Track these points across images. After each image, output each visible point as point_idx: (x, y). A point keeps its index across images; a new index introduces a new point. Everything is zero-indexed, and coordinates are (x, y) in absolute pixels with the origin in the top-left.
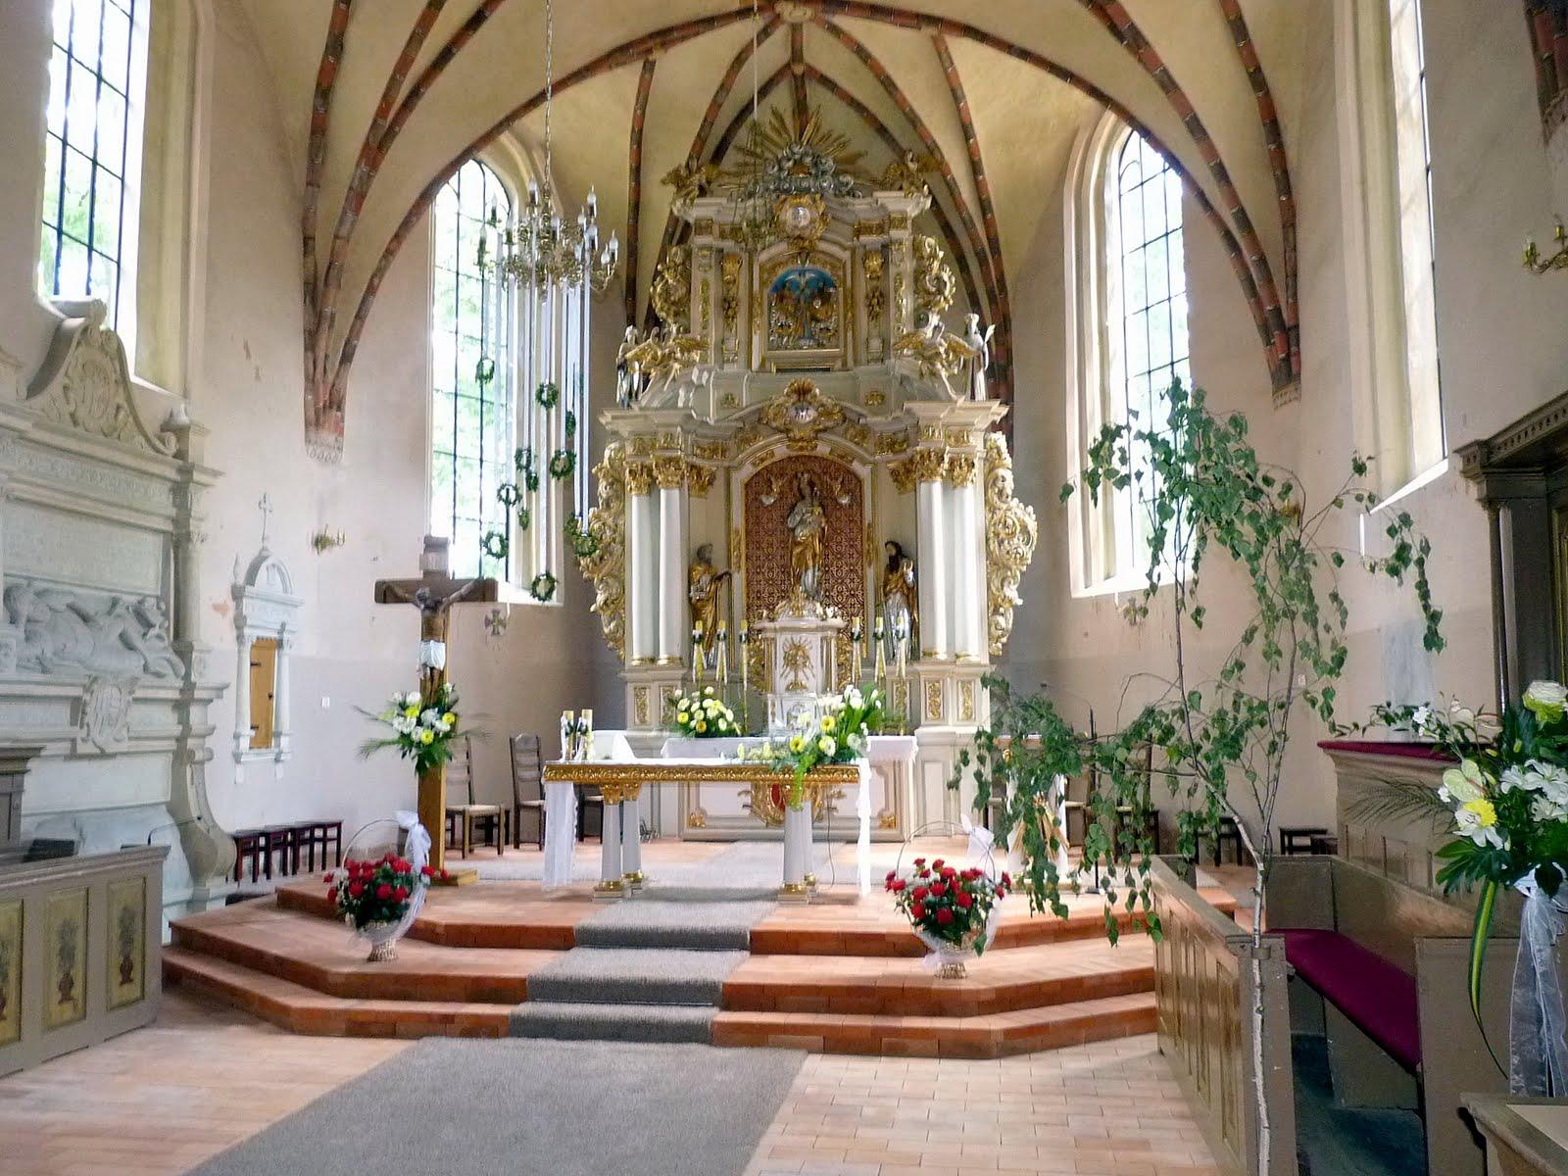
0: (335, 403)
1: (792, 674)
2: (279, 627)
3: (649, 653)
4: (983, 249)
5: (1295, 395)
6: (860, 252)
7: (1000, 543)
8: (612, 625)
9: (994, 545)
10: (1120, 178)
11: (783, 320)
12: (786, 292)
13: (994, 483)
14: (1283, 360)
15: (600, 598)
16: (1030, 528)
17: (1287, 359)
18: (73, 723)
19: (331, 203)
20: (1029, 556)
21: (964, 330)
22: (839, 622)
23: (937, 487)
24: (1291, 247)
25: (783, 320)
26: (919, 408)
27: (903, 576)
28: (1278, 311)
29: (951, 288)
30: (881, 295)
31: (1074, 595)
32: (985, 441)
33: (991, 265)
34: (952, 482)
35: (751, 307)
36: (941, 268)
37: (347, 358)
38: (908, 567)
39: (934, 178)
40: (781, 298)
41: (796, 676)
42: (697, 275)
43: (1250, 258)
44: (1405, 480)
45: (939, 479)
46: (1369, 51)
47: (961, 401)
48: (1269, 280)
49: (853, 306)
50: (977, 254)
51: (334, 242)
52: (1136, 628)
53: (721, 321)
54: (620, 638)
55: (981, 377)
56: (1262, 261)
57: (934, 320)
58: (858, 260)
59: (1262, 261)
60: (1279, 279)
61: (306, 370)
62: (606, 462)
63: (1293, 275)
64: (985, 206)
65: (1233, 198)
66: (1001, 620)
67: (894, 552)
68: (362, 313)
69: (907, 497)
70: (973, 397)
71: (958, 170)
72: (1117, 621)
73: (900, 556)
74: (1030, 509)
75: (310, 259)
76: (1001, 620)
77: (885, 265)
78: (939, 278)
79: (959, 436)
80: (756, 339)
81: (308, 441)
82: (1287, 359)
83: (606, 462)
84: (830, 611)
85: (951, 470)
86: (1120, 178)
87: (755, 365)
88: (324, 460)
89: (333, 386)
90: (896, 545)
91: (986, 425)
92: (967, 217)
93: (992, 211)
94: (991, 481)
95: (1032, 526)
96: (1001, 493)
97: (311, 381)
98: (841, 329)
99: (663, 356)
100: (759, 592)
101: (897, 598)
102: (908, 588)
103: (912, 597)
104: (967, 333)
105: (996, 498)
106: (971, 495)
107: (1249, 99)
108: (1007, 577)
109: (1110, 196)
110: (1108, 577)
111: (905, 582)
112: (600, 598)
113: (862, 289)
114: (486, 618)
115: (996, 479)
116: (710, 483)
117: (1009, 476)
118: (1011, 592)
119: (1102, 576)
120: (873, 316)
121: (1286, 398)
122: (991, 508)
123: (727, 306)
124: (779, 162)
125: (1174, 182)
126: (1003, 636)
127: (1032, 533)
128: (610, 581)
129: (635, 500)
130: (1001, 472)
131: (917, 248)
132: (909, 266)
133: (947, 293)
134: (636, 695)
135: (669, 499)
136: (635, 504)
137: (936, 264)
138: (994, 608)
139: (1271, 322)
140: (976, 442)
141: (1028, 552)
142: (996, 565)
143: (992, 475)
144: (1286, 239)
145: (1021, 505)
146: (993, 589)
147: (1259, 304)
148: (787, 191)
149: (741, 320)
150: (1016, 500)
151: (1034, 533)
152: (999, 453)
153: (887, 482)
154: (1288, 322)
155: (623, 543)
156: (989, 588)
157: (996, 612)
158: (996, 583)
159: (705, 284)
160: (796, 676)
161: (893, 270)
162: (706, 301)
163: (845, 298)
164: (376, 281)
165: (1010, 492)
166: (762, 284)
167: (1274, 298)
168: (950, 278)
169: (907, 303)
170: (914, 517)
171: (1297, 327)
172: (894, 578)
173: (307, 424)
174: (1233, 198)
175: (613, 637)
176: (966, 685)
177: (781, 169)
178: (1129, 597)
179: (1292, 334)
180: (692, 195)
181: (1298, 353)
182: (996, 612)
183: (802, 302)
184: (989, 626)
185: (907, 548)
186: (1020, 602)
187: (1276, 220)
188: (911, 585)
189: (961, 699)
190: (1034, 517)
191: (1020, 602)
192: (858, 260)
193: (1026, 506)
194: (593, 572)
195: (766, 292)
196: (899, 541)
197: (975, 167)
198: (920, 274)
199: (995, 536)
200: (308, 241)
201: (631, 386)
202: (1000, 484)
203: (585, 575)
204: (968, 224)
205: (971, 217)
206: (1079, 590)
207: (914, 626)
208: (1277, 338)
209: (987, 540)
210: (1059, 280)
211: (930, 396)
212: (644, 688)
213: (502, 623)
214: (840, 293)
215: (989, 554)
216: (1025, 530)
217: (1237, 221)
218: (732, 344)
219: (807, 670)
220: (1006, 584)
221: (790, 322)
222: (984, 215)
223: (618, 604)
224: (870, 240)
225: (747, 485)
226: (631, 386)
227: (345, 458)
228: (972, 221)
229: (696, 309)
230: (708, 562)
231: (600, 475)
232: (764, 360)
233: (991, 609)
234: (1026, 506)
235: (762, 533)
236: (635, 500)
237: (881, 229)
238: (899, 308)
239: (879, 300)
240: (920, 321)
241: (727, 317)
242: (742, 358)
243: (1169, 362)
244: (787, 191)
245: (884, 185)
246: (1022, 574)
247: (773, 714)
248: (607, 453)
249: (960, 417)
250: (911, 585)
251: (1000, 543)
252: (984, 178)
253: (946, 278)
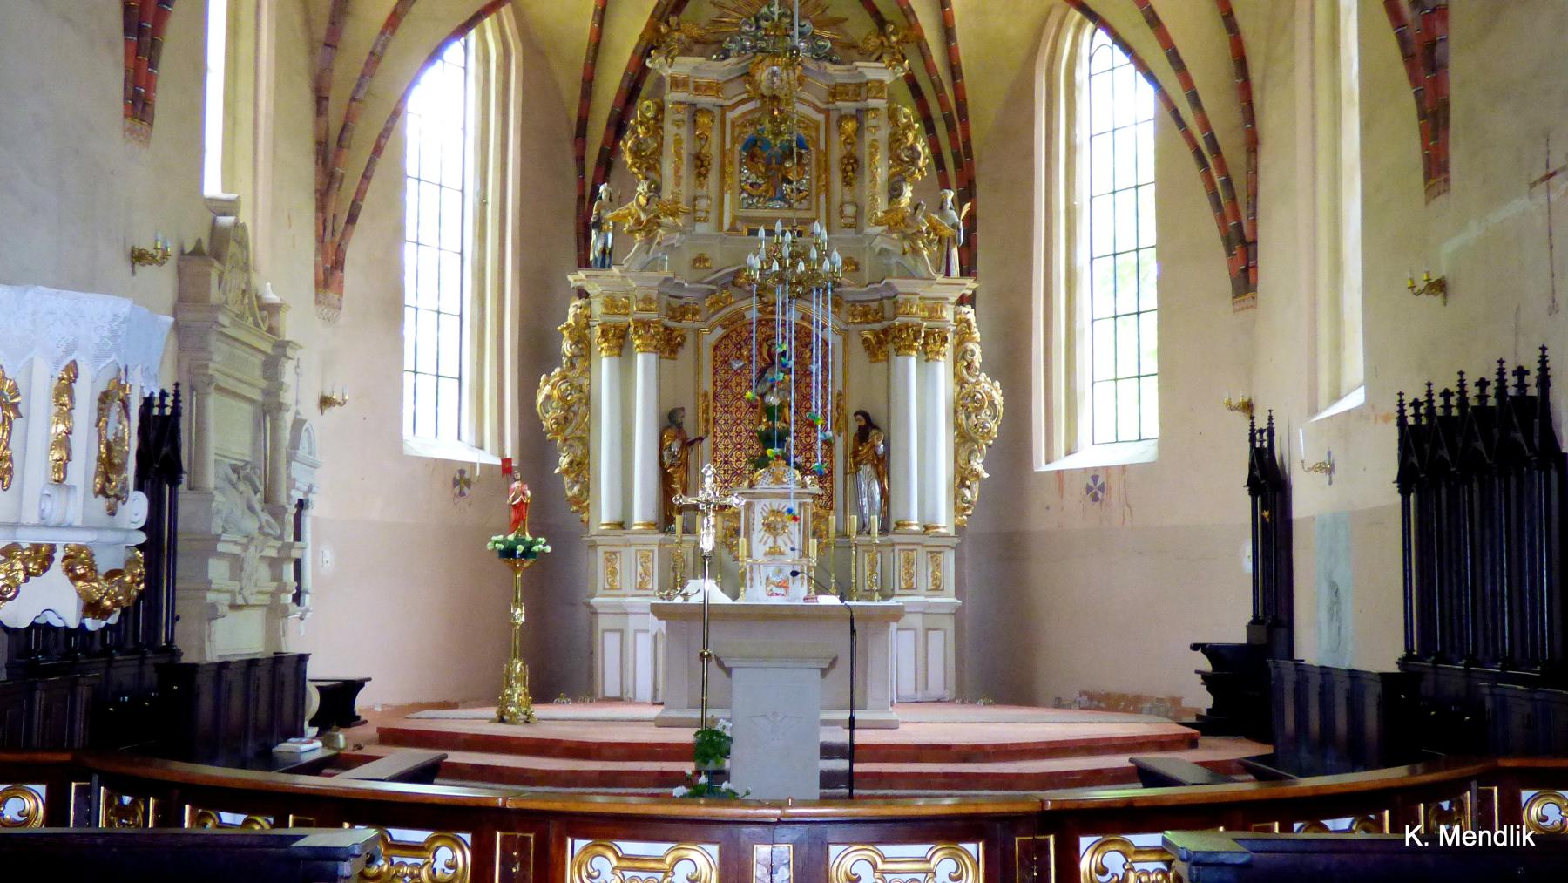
0: (338, 265)
1: (771, 539)
2: (306, 488)
3: (618, 519)
4: (951, 114)
5: (1251, 302)
6: (834, 116)
7: (968, 416)
8: (576, 489)
9: (962, 416)
10: (1091, 58)
11: (753, 178)
12: (757, 151)
13: (963, 358)
14: (1242, 270)
15: (564, 461)
16: (996, 402)
17: (1246, 270)
18: (233, 578)
19: (347, 68)
20: (995, 429)
21: (939, 205)
22: (816, 489)
23: (913, 361)
24: (1253, 171)
25: (753, 178)
26: (901, 285)
27: (874, 447)
28: (1239, 226)
29: (925, 158)
30: (856, 161)
31: (1035, 470)
32: (956, 313)
33: (959, 130)
34: (928, 355)
35: (723, 166)
36: (916, 138)
37: (352, 219)
38: (878, 440)
39: (910, 49)
40: (752, 157)
41: (775, 542)
42: (670, 130)
43: (1218, 179)
44: (1336, 397)
45: (914, 353)
46: (1322, 32)
47: (940, 278)
48: (1233, 199)
49: (827, 170)
50: (945, 117)
51: (349, 105)
52: (1098, 503)
53: (693, 179)
54: (583, 501)
55: (955, 252)
56: (1228, 182)
57: (908, 192)
58: (833, 123)
59: (1228, 182)
60: (1242, 198)
61: (317, 231)
62: (571, 320)
63: (1253, 195)
64: (955, 70)
65: (1205, 125)
66: (967, 493)
67: (863, 423)
68: (369, 174)
69: (880, 366)
70: (948, 274)
71: (932, 36)
72: (1076, 492)
73: (868, 427)
74: (997, 383)
75: (323, 119)
76: (967, 493)
77: (859, 131)
78: (913, 148)
79: (934, 312)
80: (727, 198)
81: (318, 302)
82: (1246, 270)
83: (571, 320)
84: (808, 479)
85: (925, 344)
86: (1091, 58)
87: (726, 226)
88: (328, 320)
89: (339, 245)
90: (865, 415)
91: (954, 298)
92: (936, 80)
93: (962, 77)
94: (961, 355)
95: (998, 399)
96: (969, 367)
97: (321, 240)
98: (814, 191)
99: (648, 221)
100: (726, 456)
101: (866, 469)
102: (878, 458)
103: (882, 466)
104: (942, 207)
105: (964, 372)
106: (943, 369)
107: (1224, 38)
108: (975, 450)
109: (1081, 75)
110: (1069, 453)
111: (876, 453)
112: (564, 461)
113: (837, 152)
114: (454, 479)
115: (965, 352)
116: (680, 344)
117: (978, 350)
118: (978, 465)
119: (1063, 453)
120: (847, 182)
121: (1243, 305)
122: (961, 382)
123: (700, 164)
124: (757, 20)
125: (1147, 91)
126: (968, 508)
127: (999, 407)
128: (576, 443)
129: (605, 362)
130: (971, 346)
131: (893, 116)
132: (883, 133)
133: (920, 163)
134: (608, 560)
135: (643, 363)
136: (605, 367)
137: (911, 135)
138: (962, 478)
139: (1233, 235)
140: (948, 314)
141: (994, 426)
142: (964, 438)
143: (961, 349)
144: (1248, 163)
145: (989, 379)
146: (961, 462)
147: (1222, 219)
148: (762, 50)
149: (713, 177)
150: (983, 374)
151: (1000, 409)
152: (969, 326)
153: (859, 354)
154: (1249, 238)
155: (587, 404)
156: (956, 461)
157: (962, 484)
158: (963, 455)
159: (678, 141)
160: (775, 542)
161: (868, 137)
162: (678, 154)
163: (818, 161)
164: (383, 141)
165: (977, 365)
166: (734, 140)
167: (1237, 215)
168: (923, 148)
169: (881, 170)
170: (889, 388)
171: (1255, 242)
172: (864, 450)
173: (317, 285)
174: (1205, 125)
175: (577, 500)
176: (935, 553)
177: (758, 28)
178: (1092, 474)
179: (1251, 248)
180: (673, 54)
181: (1255, 266)
182: (962, 484)
183: (774, 162)
184: (956, 498)
185: (878, 417)
186: (986, 475)
187: (1236, 116)
188: (881, 457)
189: (930, 570)
190: (1000, 391)
191: (986, 475)
192: (833, 123)
193: (993, 381)
194: (557, 433)
195: (738, 147)
196: (869, 411)
197: (948, 32)
198: (895, 140)
199: (966, 403)
200: (321, 100)
201: (605, 245)
202: (969, 357)
203: (549, 436)
204: (938, 88)
205: (940, 81)
206: (1041, 466)
207: (885, 495)
208: (1238, 251)
209: (956, 412)
210: (1029, 154)
211: (910, 275)
212: (614, 553)
213: (468, 483)
214: (812, 156)
215: (957, 426)
216: (992, 404)
217: (1207, 143)
218: (703, 204)
219: (785, 537)
220: (972, 457)
221: (760, 181)
222: (954, 79)
223: (582, 466)
224: (847, 106)
225: (716, 348)
226: (605, 245)
227: (344, 318)
228: (942, 85)
229: (668, 167)
230: (680, 426)
231: (566, 333)
232: (735, 219)
233: (958, 481)
234: (993, 381)
235: (730, 397)
236: (605, 362)
237: (856, 96)
238: (873, 175)
239: (853, 167)
240: (894, 193)
241: (699, 175)
242: (713, 216)
243: (1135, 248)
244: (762, 50)
245: (865, 55)
246: (989, 447)
247: (752, 579)
248: (571, 310)
249: (935, 291)
250: (881, 457)
251: (968, 416)
252: (956, 44)
253: (920, 149)
